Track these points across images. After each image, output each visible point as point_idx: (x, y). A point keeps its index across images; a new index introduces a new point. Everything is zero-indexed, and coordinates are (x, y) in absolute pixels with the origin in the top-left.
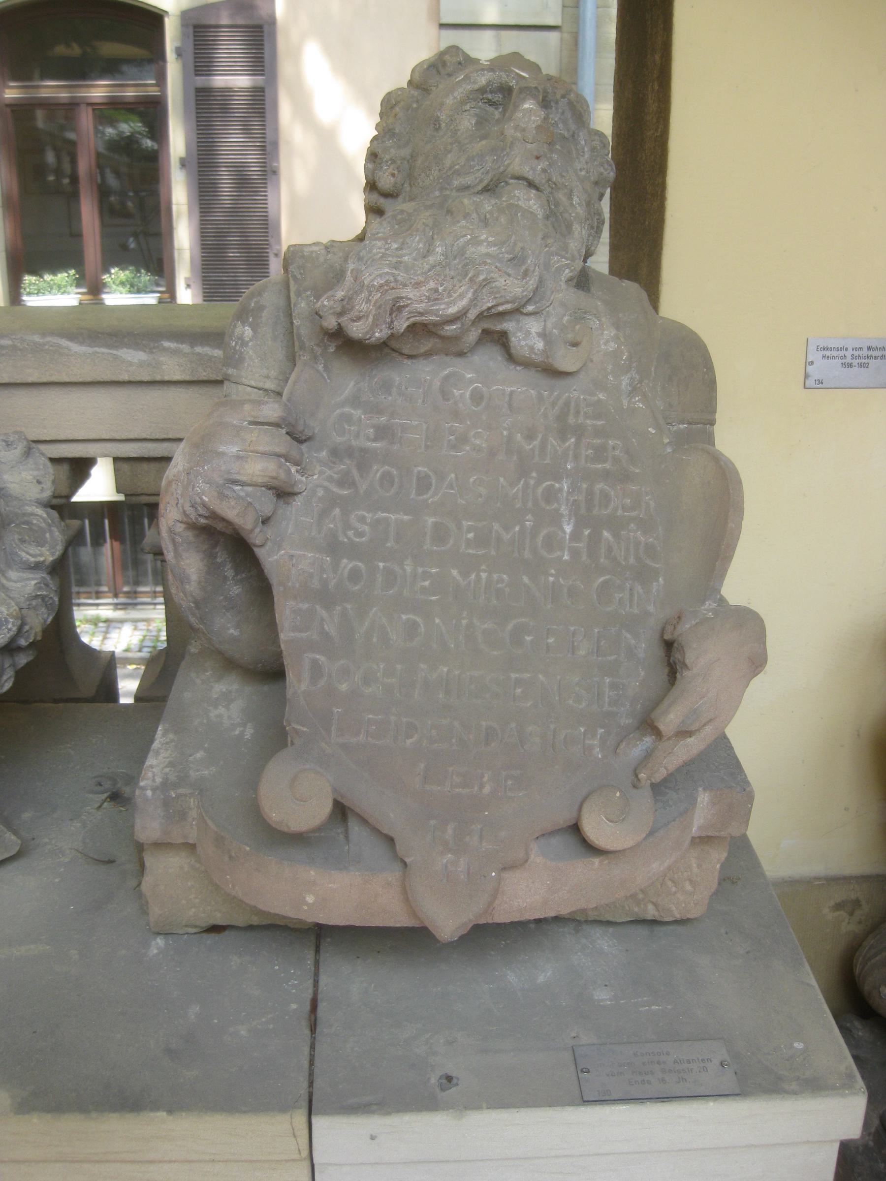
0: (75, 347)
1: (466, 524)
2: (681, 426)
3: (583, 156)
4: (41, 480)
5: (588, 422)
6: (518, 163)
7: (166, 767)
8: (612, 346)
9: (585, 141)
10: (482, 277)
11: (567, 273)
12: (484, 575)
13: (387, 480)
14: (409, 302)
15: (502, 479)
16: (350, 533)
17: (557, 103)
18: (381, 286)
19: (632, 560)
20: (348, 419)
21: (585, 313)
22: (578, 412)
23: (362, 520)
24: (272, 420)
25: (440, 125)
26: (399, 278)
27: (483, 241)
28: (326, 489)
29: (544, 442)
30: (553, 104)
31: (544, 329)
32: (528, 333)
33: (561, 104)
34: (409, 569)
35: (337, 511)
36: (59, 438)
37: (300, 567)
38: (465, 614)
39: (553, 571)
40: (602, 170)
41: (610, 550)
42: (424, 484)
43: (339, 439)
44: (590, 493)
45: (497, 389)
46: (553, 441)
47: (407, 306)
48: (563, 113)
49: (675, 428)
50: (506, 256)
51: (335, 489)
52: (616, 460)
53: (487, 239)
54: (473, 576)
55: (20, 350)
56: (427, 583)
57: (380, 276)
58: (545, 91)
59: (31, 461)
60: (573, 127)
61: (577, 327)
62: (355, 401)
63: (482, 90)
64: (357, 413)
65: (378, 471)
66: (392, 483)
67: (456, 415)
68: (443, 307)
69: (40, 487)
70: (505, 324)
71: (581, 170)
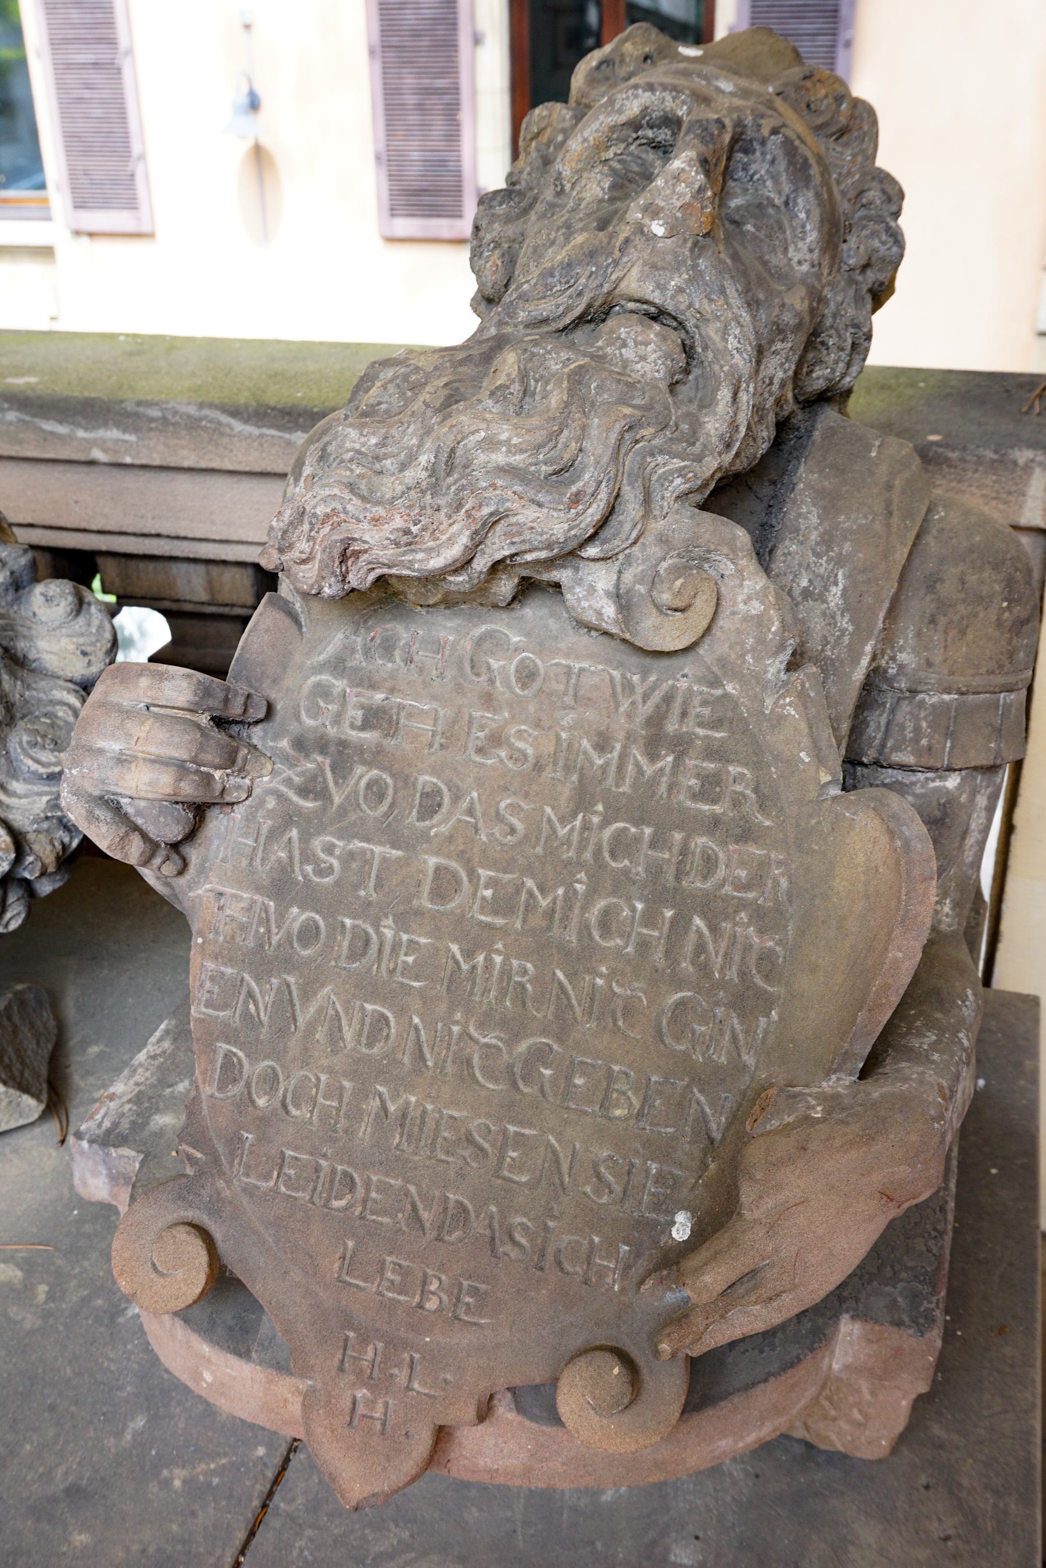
0: (238, 426)
1: (484, 873)
2: (946, 697)
3: (803, 239)
4: (88, 649)
5: (701, 732)
6: (635, 282)
7: (129, 1101)
8: (756, 608)
9: (808, 212)
10: (486, 511)
11: (679, 484)
12: (498, 959)
13: (376, 790)
14: (366, 546)
15: (548, 810)
16: (309, 869)
17: (763, 142)
18: (327, 516)
19: (732, 974)
20: (323, 692)
21: (709, 552)
22: (684, 714)
23: (329, 849)
24: (179, 704)
25: (563, 186)
26: (349, 507)
27: (500, 443)
28: (280, 796)
29: (623, 756)
30: (756, 145)
31: (617, 586)
32: (592, 590)
33: (769, 145)
34: (389, 933)
35: (294, 833)
36: (231, 538)
37: (228, 912)
38: (458, 1016)
39: (604, 969)
40: (876, 243)
41: (701, 948)
42: (430, 804)
43: (309, 722)
44: (684, 851)
45: (558, 664)
46: (637, 753)
47: (366, 551)
48: (773, 162)
49: (935, 699)
50: (544, 468)
51: (295, 798)
52: (737, 802)
53: (509, 440)
54: (481, 958)
55: (173, 424)
56: (410, 959)
57: (324, 500)
58: (739, 124)
59: (81, 620)
60: (787, 188)
61: (679, 583)
62: (338, 665)
63: (635, 125)
64: (339, 684)
65: (363, 775)
66: (381, 797)
67: (488, 700)
68: (420, 556)
69: (86, 660)
70: (555, 573)
71: (800, 263)
